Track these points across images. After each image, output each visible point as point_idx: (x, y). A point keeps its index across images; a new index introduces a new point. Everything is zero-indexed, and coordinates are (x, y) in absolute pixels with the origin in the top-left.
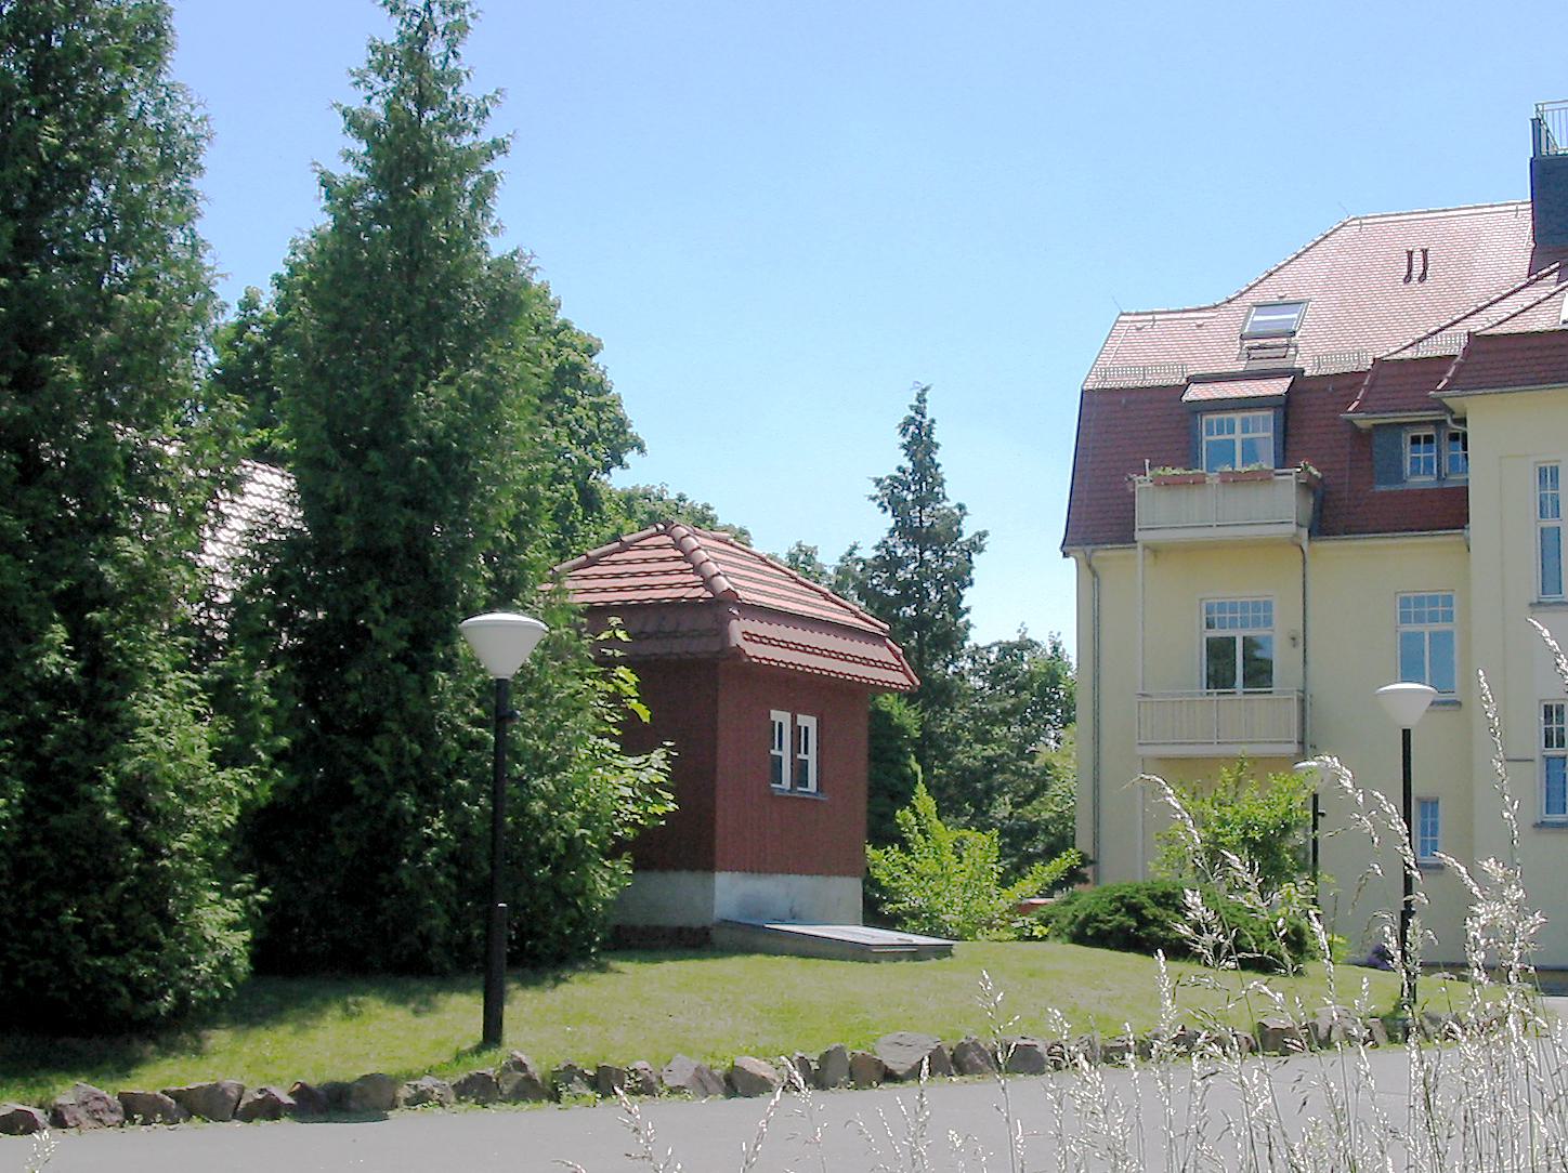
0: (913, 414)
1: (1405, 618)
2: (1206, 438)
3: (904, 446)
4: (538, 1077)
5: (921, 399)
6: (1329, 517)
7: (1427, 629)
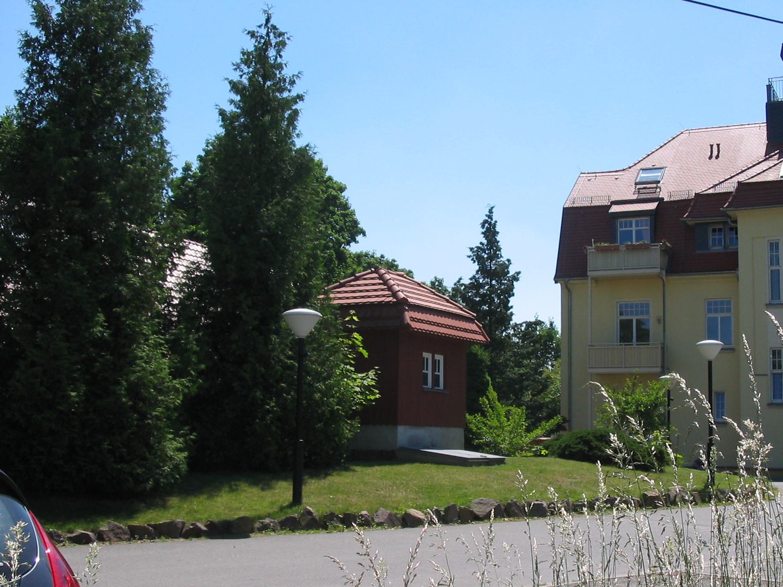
0: (487, 218)
1: (709, 311)
2: (619, 229)
3: (483, 233)
4: (317, 518)
5: (491, 211)
7: (719, 316)
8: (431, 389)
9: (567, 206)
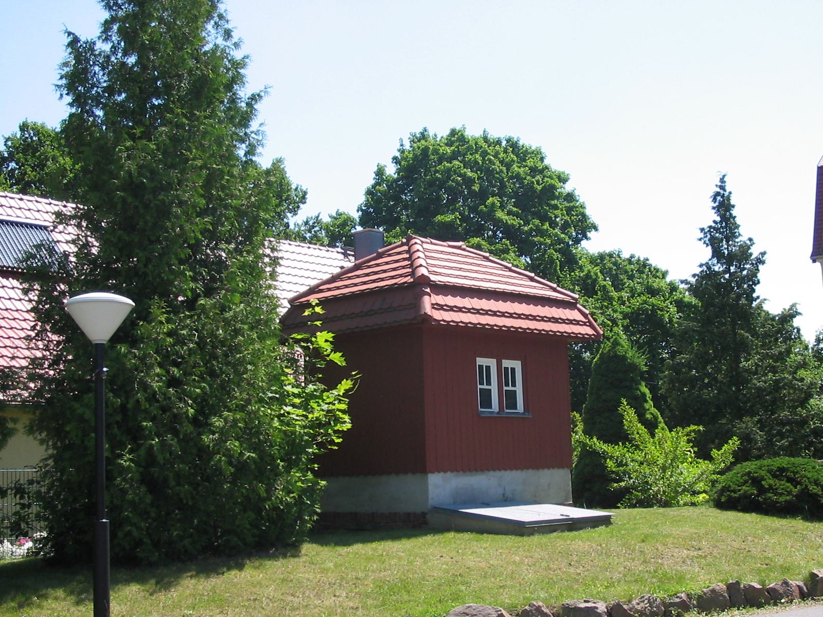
0: (718, 190)
3: (714, 208)
5: (722, 180)
8: (498, 413)
9: (819, 165)
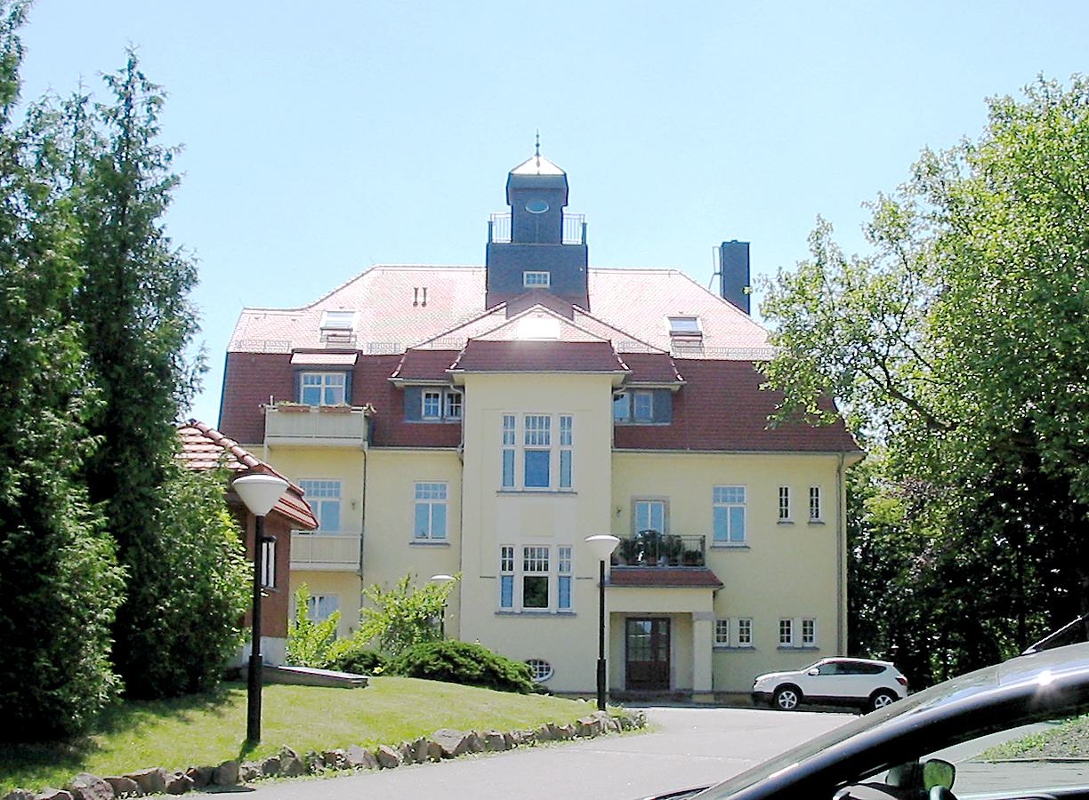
1: (418, 496)
2: (303, 386)
6: (378, 436)
7: (430, 502)
9: (231, 350)
